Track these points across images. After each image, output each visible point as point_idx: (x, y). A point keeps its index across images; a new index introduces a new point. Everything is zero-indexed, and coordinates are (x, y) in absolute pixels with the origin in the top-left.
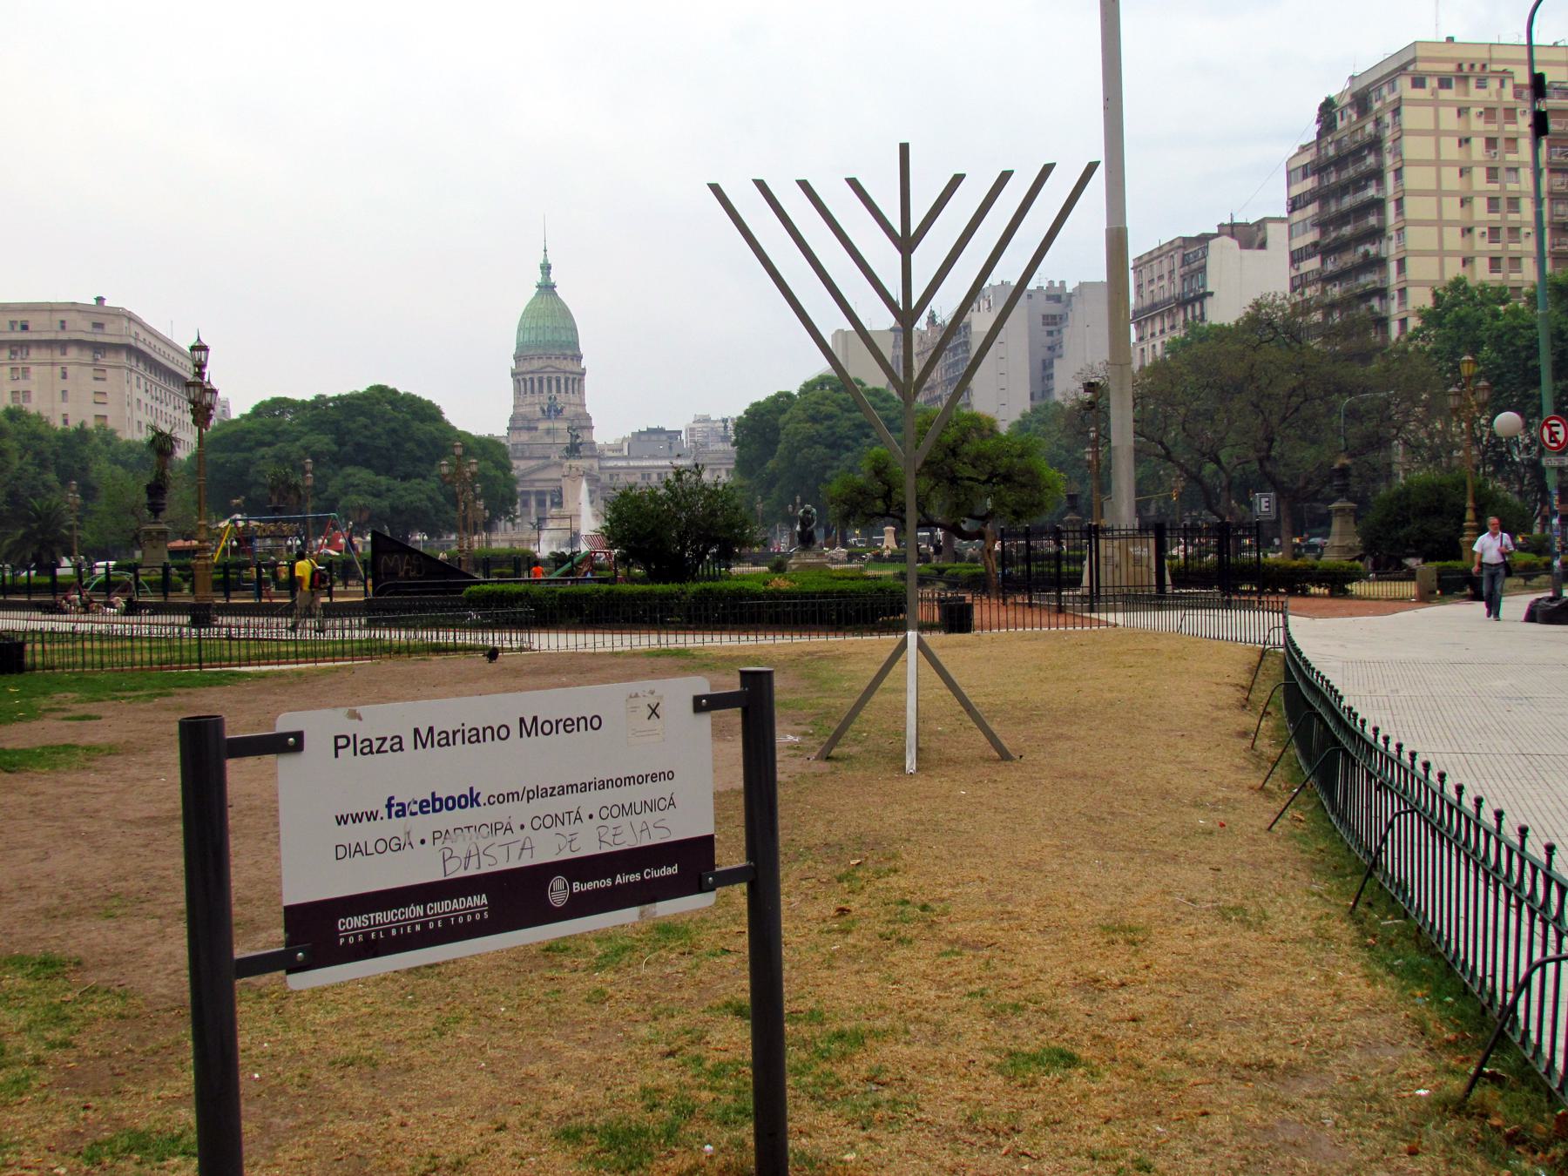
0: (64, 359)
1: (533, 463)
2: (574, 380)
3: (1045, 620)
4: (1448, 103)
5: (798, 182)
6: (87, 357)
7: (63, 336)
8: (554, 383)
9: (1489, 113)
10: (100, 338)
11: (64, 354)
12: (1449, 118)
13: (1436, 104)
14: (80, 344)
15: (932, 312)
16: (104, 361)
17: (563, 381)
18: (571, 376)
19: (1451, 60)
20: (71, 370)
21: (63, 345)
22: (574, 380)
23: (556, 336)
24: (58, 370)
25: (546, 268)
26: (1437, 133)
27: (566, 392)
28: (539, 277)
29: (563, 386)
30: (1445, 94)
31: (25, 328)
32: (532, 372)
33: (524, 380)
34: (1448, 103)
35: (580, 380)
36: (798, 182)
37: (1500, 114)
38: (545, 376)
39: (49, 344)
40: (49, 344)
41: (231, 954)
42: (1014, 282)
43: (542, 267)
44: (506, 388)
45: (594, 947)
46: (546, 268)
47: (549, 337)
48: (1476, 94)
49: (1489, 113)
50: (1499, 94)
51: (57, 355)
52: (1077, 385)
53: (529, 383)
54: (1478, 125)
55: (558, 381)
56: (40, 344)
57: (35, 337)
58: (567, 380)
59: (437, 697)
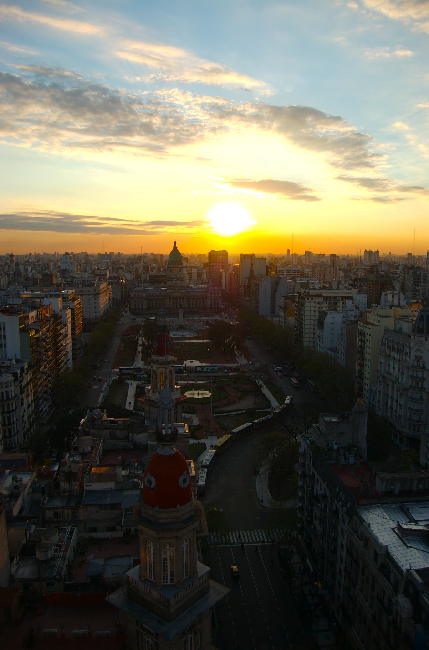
0: (89, 297)
1: (172, 291)
4: (313, 302)
6: (93, 296)
7: (89, 293)
9: (319, 303)
10: (95, 293)
11: (89, 296)
12: (313, 304)
13: (311, 302)
14: (92, 294)
16: (96, 296)
17: (178, 270)
18: (180, 268)
19: (315, 293)
20: (90, 299)
21: (89, 295)
24: (88, 299)
25: (175, 243)
26: (310, 306)
28: (174, 245)
30: (312, 300)
31: (82, 291)
32: (172, 268)
34: (313, 302)
37: (321, 303)
39: (87, 294)
40: (87, 294)
41: (210, 570)
43: (174, 243)
45: (208, 105)
46: (175, 243)
48: (317, 300)
49: (319, 303)
50: (321, 300)
51: (88, 296)
54: (317, 305)
56: (85, 294)
57: (84, 293)
58: (179, 269)
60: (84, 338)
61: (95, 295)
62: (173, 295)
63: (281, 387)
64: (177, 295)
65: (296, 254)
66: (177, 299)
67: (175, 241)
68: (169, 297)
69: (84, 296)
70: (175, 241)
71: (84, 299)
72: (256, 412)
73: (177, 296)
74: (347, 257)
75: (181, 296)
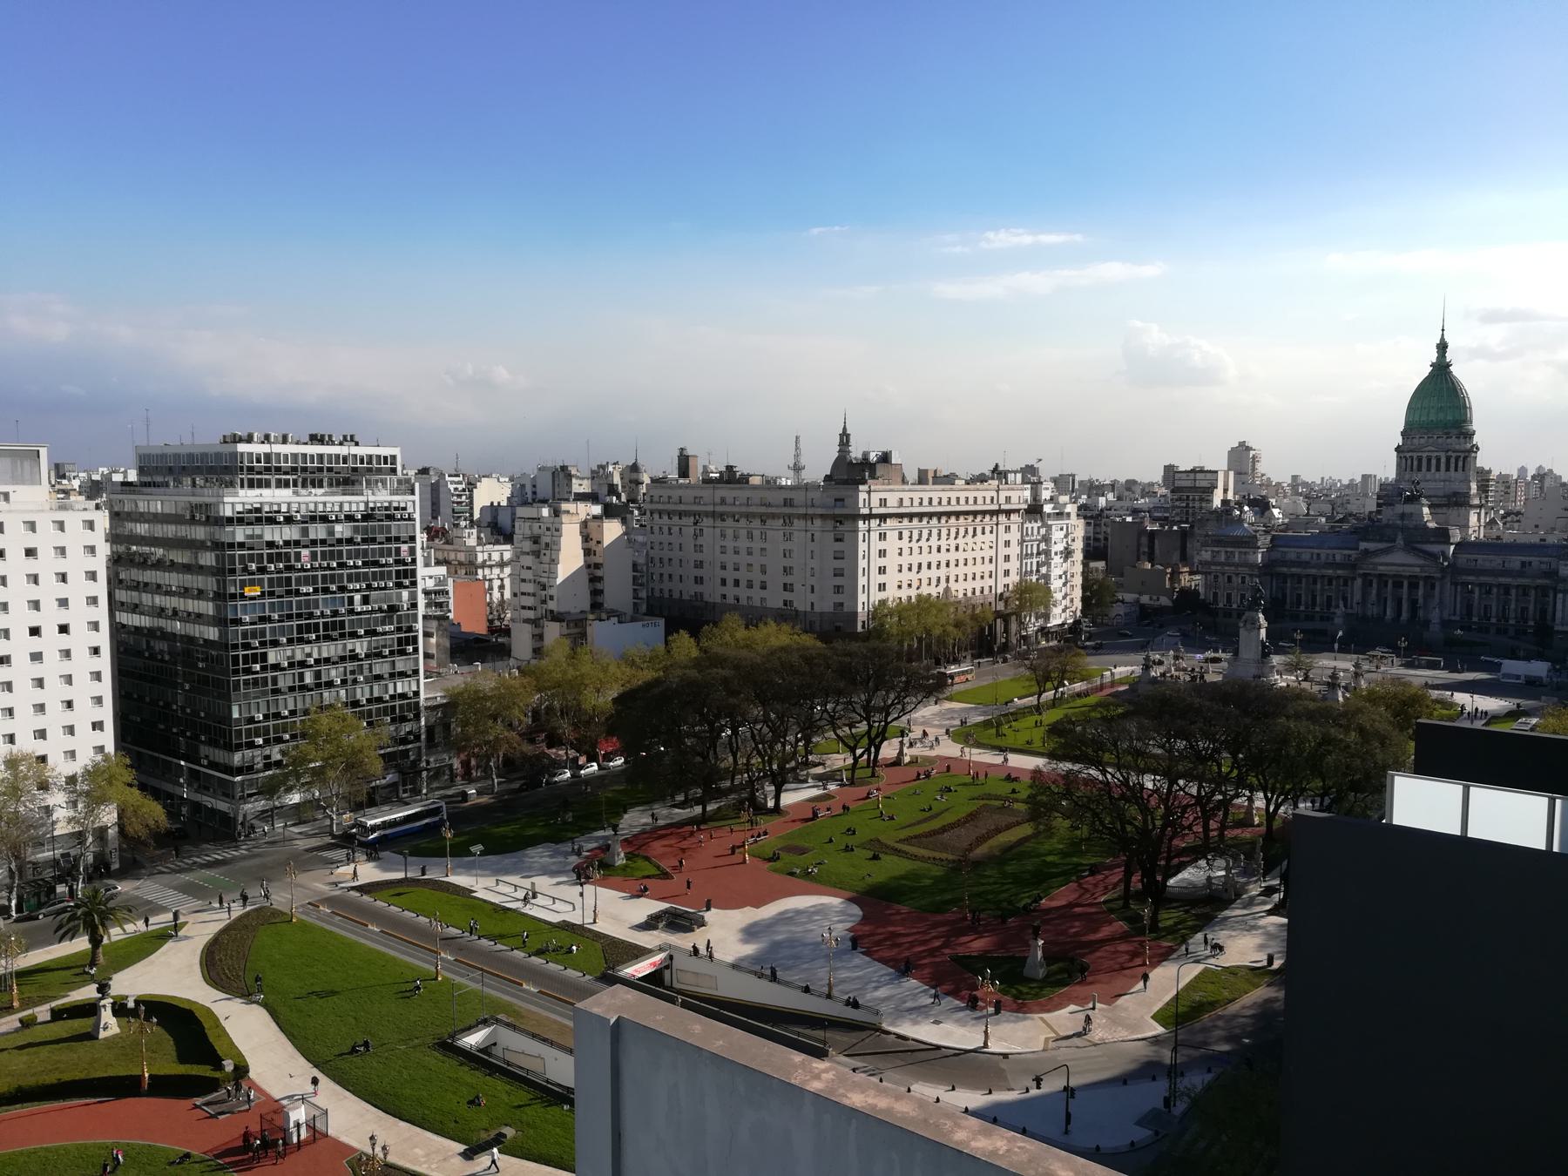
0: (725, 524)
2: (1457, 459)
3: (321, 508)
5: (71, 684)
6: (830, 524)
8: (1434, 462)
15: (435, 586)
18: (1454, 455)
22: (1457, 459)
23: (1441, 416)
24: (809, 534)
25: (1442, 347)
27: (1456, 470)
28: (1433, 356)
29: (1453, 465)
33: (1412, 458)
35: (1465, 458)
36: (71, 684)
38: (1424, 455)
42: (1180, 470)
44: (1393, 457)
46: (1442, 347)
47: (1432, 417)
52: (91, 753)
53: (1409, 462)
55: (1438, 460)
59: (1100, 654)
60: (602, 772)
61: (839, 520)
62: (1382, 564)
63: (694, 947)
64: (1403, 565)
65: (1399, 458)
66: (1398, 585)
67: (845, 429)
68: (1361, 572)
69: (769, 522)
70: (845, 429)
71: (705, 529)
72: (104, 495)
73: (1401, 569)
74: (1348, 486)
75: (1418, 569)
